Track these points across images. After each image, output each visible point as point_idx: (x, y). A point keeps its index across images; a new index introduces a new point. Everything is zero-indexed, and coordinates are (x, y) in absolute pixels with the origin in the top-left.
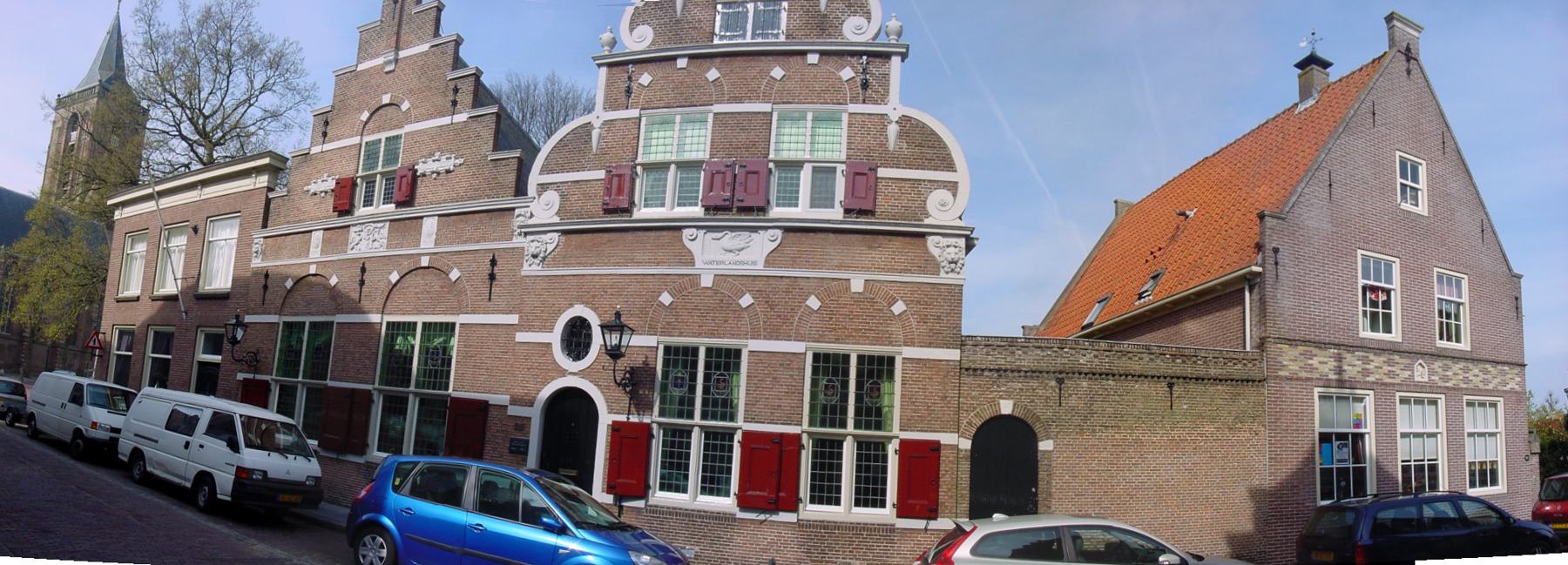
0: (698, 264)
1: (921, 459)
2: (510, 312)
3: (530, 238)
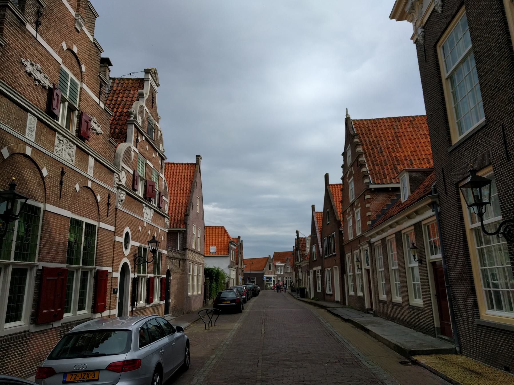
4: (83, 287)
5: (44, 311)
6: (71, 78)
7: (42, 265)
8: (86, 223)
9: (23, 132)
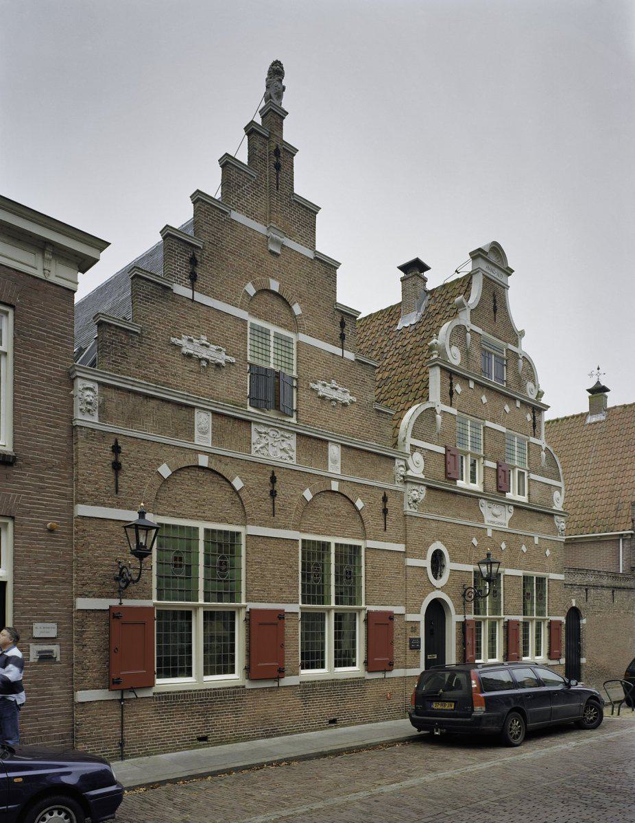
0: (486, 523)
1: (381, 625)
2: (398, 542)
3: (409, 486)
4: (538, 637)
5: (376, 659)
6: (275, 333)
7: (507, 618)
8: (337, 545)
9: (191, 436)
